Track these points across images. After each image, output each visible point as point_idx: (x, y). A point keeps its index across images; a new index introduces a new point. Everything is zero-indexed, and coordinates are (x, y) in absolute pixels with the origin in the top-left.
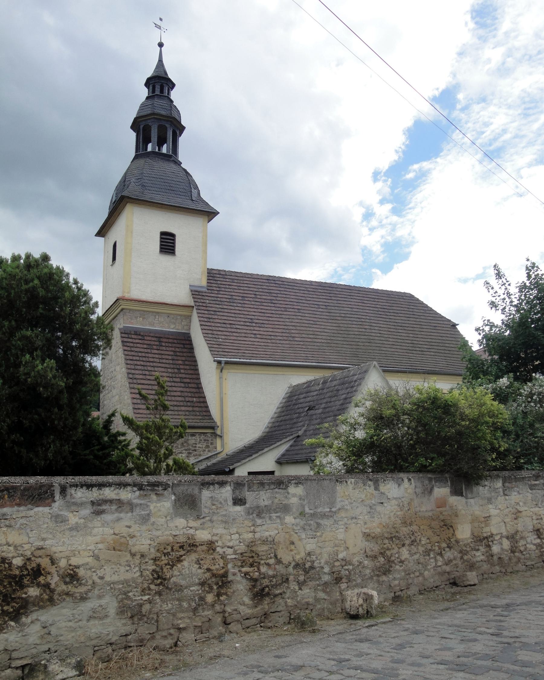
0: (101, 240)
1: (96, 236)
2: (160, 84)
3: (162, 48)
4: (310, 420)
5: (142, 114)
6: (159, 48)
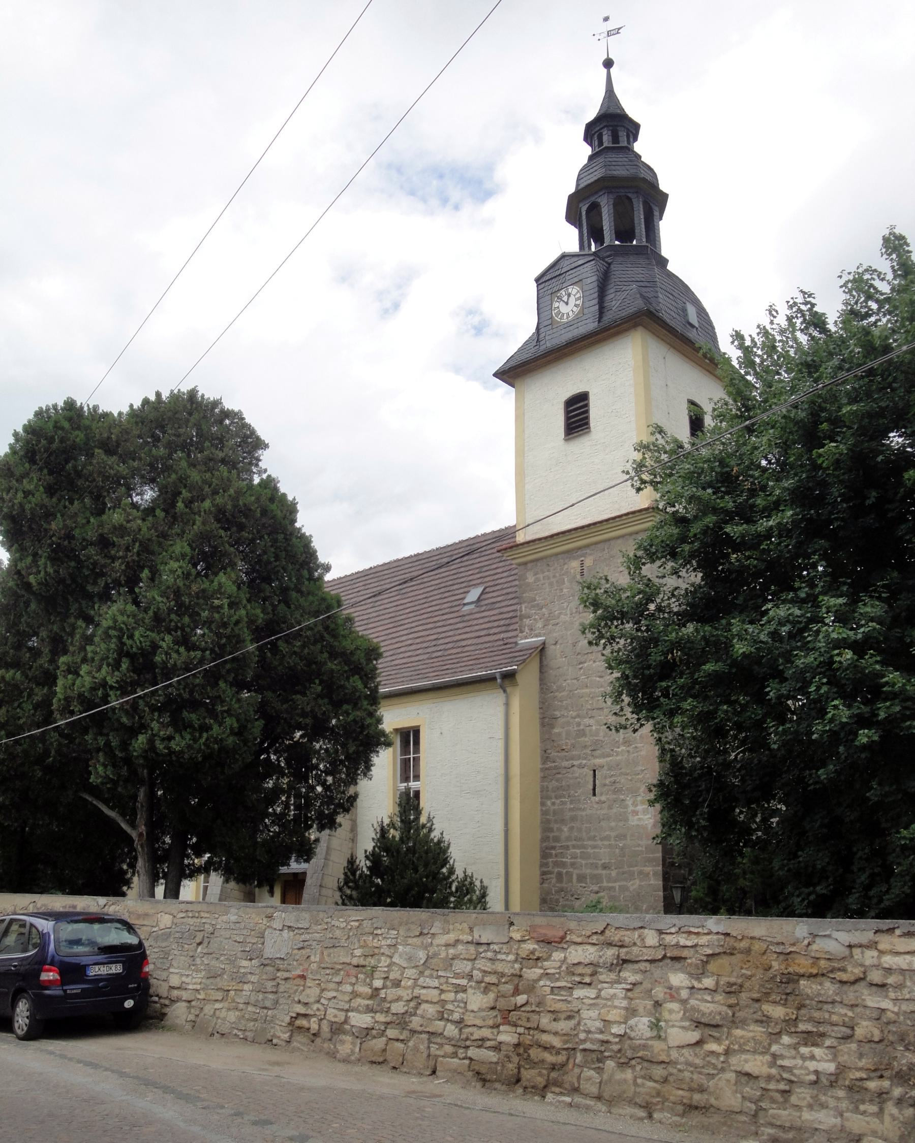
0: (504, 393)
1: (495, 375)
2: (612, 129)
3: (611, 70)
4: (592, 975)
5: (582, 186)
6: (605, 70)
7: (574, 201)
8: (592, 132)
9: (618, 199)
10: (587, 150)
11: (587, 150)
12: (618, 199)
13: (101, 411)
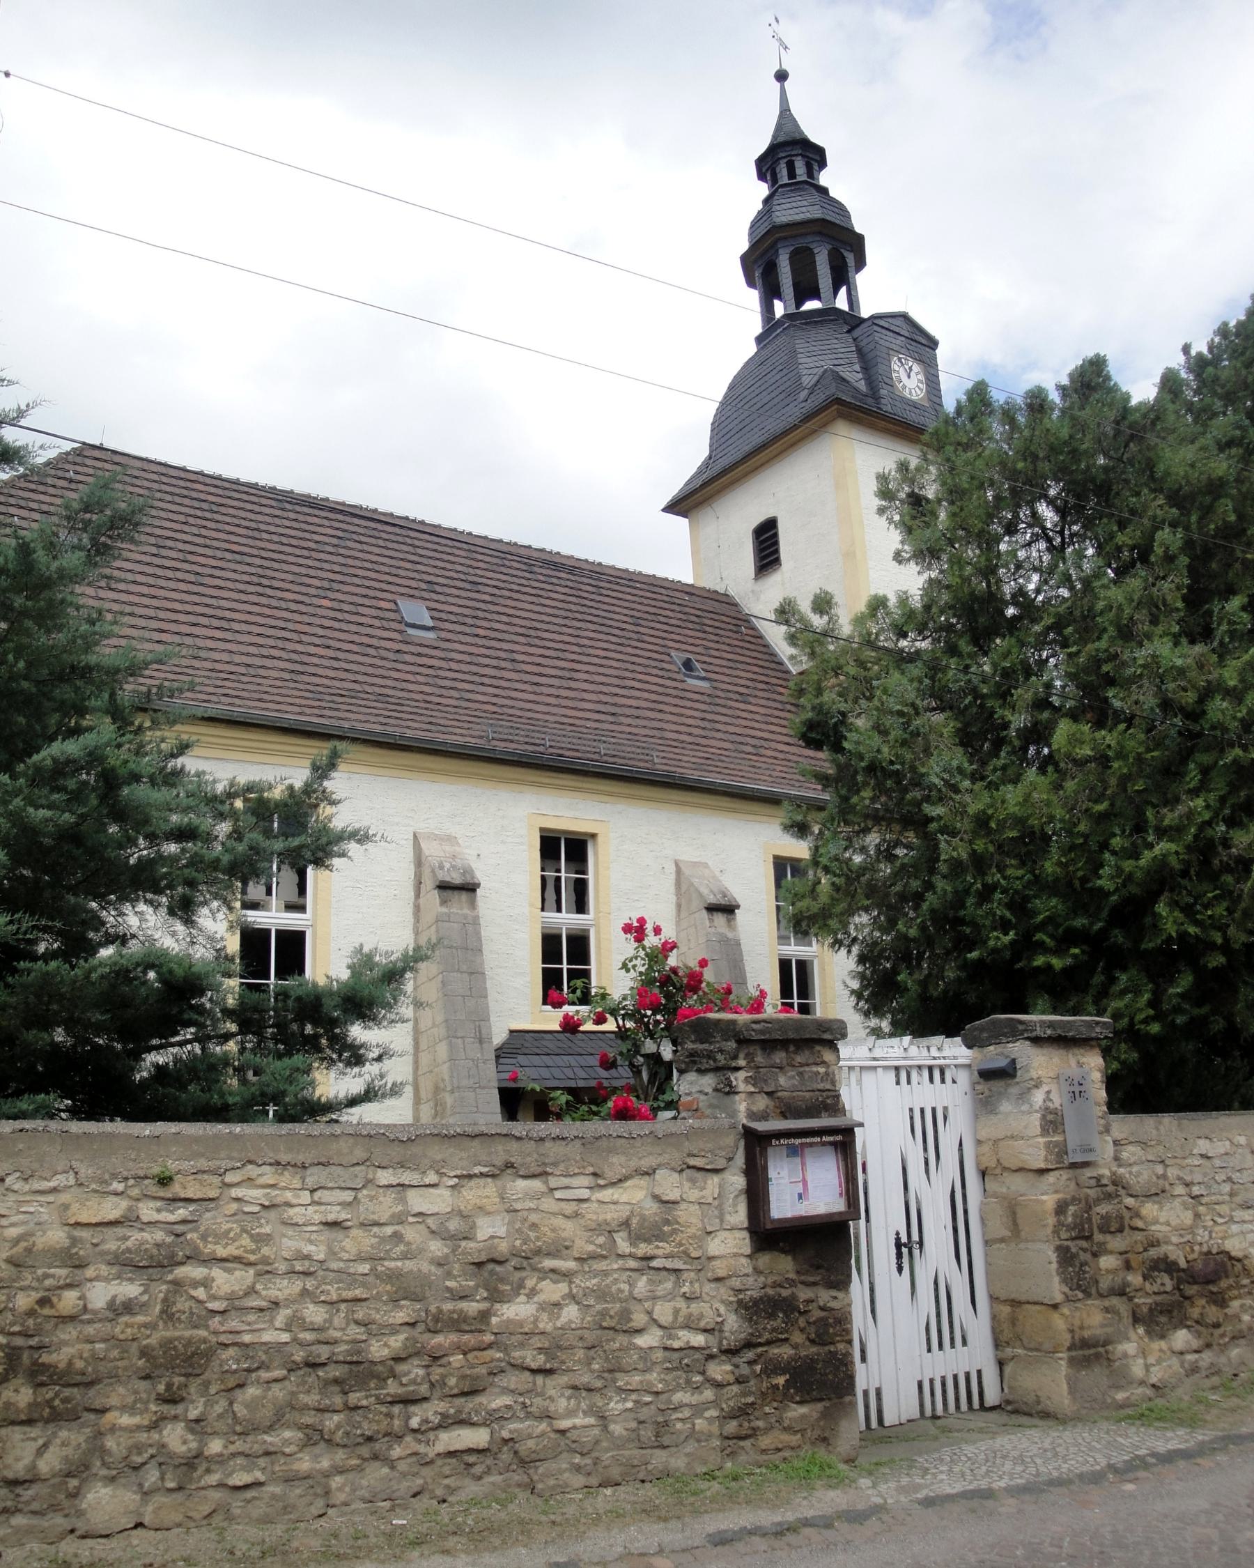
0: (680, 524)
2: (791, 159)
7: (748, 261)
8: (766, 166)
9: (802, 247)
10: (763, 190)
11: (763, 190)
12: (802, 247)
13: (1019, 401)
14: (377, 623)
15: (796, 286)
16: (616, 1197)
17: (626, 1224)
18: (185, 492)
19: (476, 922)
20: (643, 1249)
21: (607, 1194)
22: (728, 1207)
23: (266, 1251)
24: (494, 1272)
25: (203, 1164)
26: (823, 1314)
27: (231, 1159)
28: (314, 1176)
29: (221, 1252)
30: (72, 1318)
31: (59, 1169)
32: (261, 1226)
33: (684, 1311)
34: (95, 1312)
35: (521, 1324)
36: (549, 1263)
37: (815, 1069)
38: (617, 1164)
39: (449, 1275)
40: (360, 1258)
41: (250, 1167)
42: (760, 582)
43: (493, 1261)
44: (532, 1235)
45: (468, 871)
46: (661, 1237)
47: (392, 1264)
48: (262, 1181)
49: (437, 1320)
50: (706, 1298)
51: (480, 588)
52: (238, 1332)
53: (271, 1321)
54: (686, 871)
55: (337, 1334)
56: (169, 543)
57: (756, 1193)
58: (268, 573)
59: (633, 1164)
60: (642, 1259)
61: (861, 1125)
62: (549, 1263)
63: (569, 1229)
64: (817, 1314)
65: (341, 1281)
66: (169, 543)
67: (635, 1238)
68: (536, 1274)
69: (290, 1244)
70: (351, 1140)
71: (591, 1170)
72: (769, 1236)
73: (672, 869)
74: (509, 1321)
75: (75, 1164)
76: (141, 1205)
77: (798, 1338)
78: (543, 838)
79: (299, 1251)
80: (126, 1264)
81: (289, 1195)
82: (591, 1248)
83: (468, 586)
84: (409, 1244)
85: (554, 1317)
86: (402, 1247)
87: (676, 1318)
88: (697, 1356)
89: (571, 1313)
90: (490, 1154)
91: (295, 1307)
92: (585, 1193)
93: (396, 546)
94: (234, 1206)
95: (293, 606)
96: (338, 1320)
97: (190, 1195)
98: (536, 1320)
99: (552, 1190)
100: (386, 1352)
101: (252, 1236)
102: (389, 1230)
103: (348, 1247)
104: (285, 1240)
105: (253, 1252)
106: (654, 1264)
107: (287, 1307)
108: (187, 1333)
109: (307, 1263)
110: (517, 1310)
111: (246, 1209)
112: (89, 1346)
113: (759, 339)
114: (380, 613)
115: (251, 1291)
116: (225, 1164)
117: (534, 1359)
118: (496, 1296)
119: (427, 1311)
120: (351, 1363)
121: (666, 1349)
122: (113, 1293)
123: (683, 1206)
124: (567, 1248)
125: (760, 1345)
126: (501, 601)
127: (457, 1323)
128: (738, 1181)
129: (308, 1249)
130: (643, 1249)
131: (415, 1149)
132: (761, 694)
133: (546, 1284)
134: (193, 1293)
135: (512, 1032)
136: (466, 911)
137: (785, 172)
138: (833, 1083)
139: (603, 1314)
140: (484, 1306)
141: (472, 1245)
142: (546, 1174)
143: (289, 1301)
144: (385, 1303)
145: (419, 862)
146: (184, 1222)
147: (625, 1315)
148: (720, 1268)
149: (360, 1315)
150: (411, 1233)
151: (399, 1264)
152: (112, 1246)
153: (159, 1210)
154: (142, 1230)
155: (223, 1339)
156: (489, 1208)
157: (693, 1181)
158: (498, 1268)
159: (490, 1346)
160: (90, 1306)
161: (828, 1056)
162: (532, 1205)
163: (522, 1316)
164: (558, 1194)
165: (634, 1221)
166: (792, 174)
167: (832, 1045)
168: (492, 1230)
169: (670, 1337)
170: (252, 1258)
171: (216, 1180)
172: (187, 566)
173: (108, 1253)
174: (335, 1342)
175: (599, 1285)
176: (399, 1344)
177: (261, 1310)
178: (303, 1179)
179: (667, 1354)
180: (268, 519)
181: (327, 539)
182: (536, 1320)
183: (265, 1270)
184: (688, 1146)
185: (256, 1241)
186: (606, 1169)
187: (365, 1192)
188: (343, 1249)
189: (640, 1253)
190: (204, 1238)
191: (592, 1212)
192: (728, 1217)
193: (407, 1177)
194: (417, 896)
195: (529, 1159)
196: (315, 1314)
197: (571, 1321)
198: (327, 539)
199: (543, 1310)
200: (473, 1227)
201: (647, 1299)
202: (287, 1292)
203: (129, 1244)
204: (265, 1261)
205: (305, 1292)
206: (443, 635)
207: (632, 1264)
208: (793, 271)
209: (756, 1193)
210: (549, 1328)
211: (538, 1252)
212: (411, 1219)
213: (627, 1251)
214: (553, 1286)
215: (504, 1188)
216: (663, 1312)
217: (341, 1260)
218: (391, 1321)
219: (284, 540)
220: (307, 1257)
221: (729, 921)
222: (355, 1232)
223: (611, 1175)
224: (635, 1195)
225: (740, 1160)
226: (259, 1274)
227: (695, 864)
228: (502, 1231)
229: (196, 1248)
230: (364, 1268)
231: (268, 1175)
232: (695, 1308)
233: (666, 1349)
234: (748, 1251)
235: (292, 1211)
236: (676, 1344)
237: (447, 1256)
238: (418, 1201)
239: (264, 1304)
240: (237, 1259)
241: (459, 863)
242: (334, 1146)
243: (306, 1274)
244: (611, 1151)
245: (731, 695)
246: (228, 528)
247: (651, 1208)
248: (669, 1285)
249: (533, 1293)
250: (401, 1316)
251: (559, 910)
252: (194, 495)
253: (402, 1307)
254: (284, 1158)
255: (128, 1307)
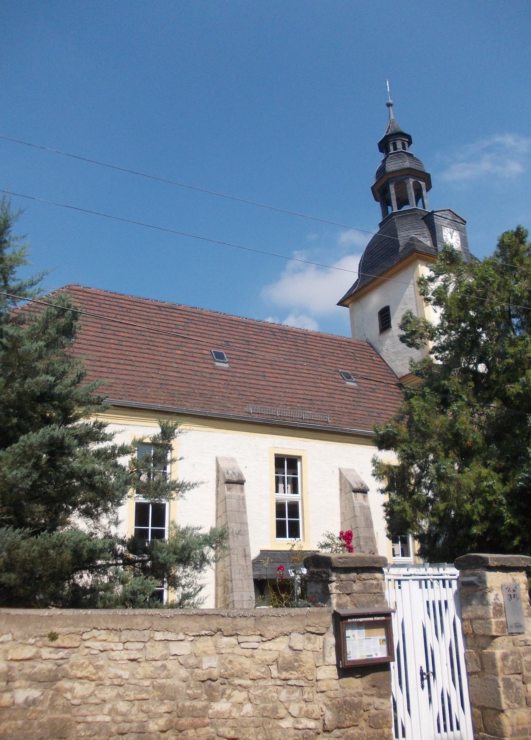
0: (345, 310)
2: (392, 142)
14: (202, 360)
15: (398, 200)
16: (271, 647)
17: (276, 661)
18: (116, 304)
19: (243, 499)
20: (285, 675)
21: (267, 645)
22: (327, 654)
23: (101, 674)
24: (212, 686)
25: (72, 629)
26: (376, 712)
27: (85, 627)
28: (125, 636)
29: (79, 674)
30: (7, 707)
31: (4, 632)
32: (99, 661)
33: (305, 709)
34: (18, 705)
35: (222, 713)
36: (237, 681)
37: (371, 581)
38: (271, 630)
39: (188, 687)
40: (146, 678)
41: (95, 631)
42: (382, 336)
43: (210, 679)
44: (229, 666)
45: (240, 474)
46: (293, 668)
47: (160, 681)
48: (100, 638)
49: (182, 711)
50: (316, 702)
51: (251, 343)
52: (85, 716)
53: (102, 709)
54: (344, 473)
55: (133, 718)
56: (108, 327)
57: (340, 648)
58: (153, 339)
59: (280, 630)
60: (283, 680)
61: (394, 612)
62: (237, 681)
63: (248, 663)
64: (373, 711)
65: (136, 690)
66: (108, 327)
67: (280, 669)
68: (231, 687)
69: (113, 671)
70: (143, 617)
71: (259, 633)
72: (348, 670)
73: (338, 472)
74: (217, 712)
75: (12, 630)
76: (42, 650)
77: (363, 724)
78: (275, 458)
79: (116, 674)
80: (34, 680)
81: (112, 645)
82: (258, 674)
83: (244, 342)
84: (169, 671)
85: (240, 710)
86: (166, 672)
87: (300, 712)
88: (311, 733)
89: (248, 708)
90: (209, 624)
91: (112, 703)
92: (255, 645)
93: (212, 325)
94: (87, 650)
95: (164, 354)
96: (134, 710)
97: (65, 645)
98: (230, 712)
99: (239, 643)
100: (156, 727)
101: (94, 666)
102: (160, 663)
103: (140, 672)
104: (110, 668)
105: (95, 674)
106: (290, 682)
107: (109, 703)
108: (61, 716)
109: (120, 680)
110: (221, 706)
111: (92, 652)
112: (14, 722)
113: (381, 225)
114: (204, 356)
115: (92, 694)
116: (82, 630)
117: (229, 732)
118: (212, 699)
119: (178, 706)
120: (140, 733)
121: (295, 729)
122: (27, 695)
123: (305, 652)
124: (247, 673)
125: (344, 728)
126: (260, 349)
127: (193, 712)
128: (331, 640)
129: (120, 672)
130: (285, 675)
131: (174, 622)
132: (382, 388)
133: (236, 693)
134: (64, 695)
135: (261, 551)
136: (239, 493)
137: (391, 148)
138: (381, 589)
139: (264, 709)
140: (204, 703)
141: (200, 671)
142: (238, 635)
143: (111, 700)
144: (157, 702)
145: (218, 470)
146: (62, 659)
147: (275, 710)
148: (322, 686)
149: (144, 708)
150: (172, 665)
151: (164, 681)
152: (27, 671)
153: (51, 653)
154: (42, 663)
155: (79, 719)
156: (209, 652)
157: (309, 639)
158: (213, 684)
159: (208, 725)
160: (16, 702)
161: (378, 575)
162: (230, 651)
163: (223, 710)
164: (243, 645)
165: (280, 660)
166: (395, 148)
167: (380, 570)
168: (210, 664)
169: (298, 722)
170: (94, 677)
171: (78, 638)
172: (116, 337)
173: (25, 674)
174: (131, 722)
175: (262, 693)
176: (163, 723)
177: (97, 704)
178: (120, 637)
179: (296, 731)
180: (154, 315)
181: (179, 323)
182: (230, 712)
183: (100, 684)
184: (306, 621)
185: (97, 669)
186: (266, 632)
187: (149, 643)
188: (137, 673)
189: (283, 677)
190: (72, 666)
191: (259, 655)
192: (327, 659)
193: (170, 636)
194: (217, 487)
195: (228, 627)
196: (122, 706)
197: (248, 713)
198: (179, 323)
199: (234, 706)
200: (201, 662)
201: (286, 702)
202: (109, 695)
203: (35, 670)
204: (100, 679)
205: (119, 696)
206: (232, 365)
207: (279, 682)
208: (396, 193)
209: (340, 648)
210: (237, 716)
211: (232, 675)
212: (171, 658)
213: (276, 676)
214: (239, 693)
215: (216, 642)
216: (294, 709)
217: (136, 678)
218: (160, 711)
219: (160, 324)
220: (120, 677)
221: (364, 497)
222: (142, 664)
223: (268, 636)
224: (280, 646)
225: (332, 629)
226: (97, 685)
227: (348, 470)
228: (214, 664)
229: (67, 672)
230: (147, 683)
231: (103, 634)
232: (310, 707)
233: (295, 729)
234: (338, 678)
235: (113, 654)
236: (300, 727)
237: (188, 677)
238: (175, 648)
239: (98, 701)
240: (87, 678)
241: (236, 471)
242: (135, 620)
243: (120, 686)
244: (269, 623)
245: (367, 389)
246: (134, 319)
247: (289, 654)
248: (297, 694)
249: (230, 697)
250: (164, 708)
251: (285, 493)
252: (120, 305)
253: (164, 704)
254: (111, 626)
255: (34, 702)
